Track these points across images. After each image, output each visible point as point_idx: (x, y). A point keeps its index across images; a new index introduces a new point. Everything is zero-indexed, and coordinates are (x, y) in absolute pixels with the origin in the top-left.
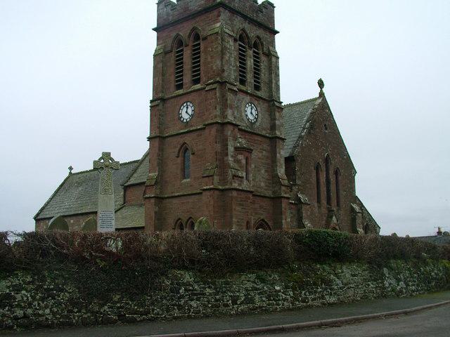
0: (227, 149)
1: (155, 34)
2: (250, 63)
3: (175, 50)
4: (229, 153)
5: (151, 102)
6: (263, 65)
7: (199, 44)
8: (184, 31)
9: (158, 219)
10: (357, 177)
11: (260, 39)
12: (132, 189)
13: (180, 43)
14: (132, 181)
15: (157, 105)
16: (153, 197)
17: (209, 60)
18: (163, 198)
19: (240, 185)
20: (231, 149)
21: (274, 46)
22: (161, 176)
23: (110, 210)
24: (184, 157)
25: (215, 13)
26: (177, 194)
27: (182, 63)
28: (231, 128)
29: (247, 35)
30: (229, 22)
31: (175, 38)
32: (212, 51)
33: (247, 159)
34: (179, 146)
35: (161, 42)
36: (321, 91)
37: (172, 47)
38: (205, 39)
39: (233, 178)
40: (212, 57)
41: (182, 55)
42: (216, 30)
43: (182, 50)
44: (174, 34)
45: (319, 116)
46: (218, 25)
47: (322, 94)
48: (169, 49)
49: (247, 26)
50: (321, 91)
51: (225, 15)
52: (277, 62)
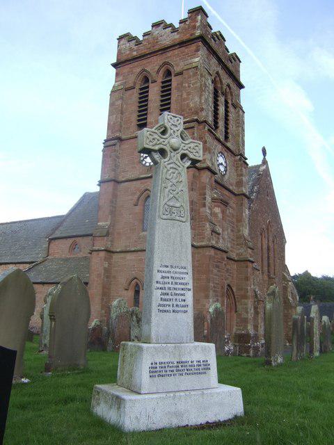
0: (205, 199)
1: (114, 70)
2: (222, 109)
3: (138, 87)
4: (207, 203)
5: (106, 141)
6: (232, 116)
7: (170, 80)
8: (153, 66)
9: (108, 277)
10: (287, 247)
11: (230, 88)
12: (57, 242)
13: (146, 80)
14: (58, 234)
15: (114, 145)
16: (103, 250)
17: (185, 95)
18: (113, 252)
19: (217, 242)
20: (209, 199)
21: (239, 99)
22: (113, 225)
23: (183, 264)
24: (144, 206)
25: (193, 47)
26: (133, 249)
27: (147, 101)
28: (208, 173)
29: (220, 79)
30: (207, 60)
31: (141, 73)
32: (189, 87)
33: (223, 212)
34: (138, 194)
35: (121, 78)
36: (264, 158)
37: (135, 83)
38: (180, 73)
39: (212, 235)
40: (188, 94)
41: (148, 92)
42: (194, 65)
43: (148, 87)
44: (138, 70)
45: (262, 178)
46: (197, 60)
47: (265, 162)
48: (131, 85)
49: (222, 72)
50: (264, 158)
51: (203, 51)
52: (243, 117)
